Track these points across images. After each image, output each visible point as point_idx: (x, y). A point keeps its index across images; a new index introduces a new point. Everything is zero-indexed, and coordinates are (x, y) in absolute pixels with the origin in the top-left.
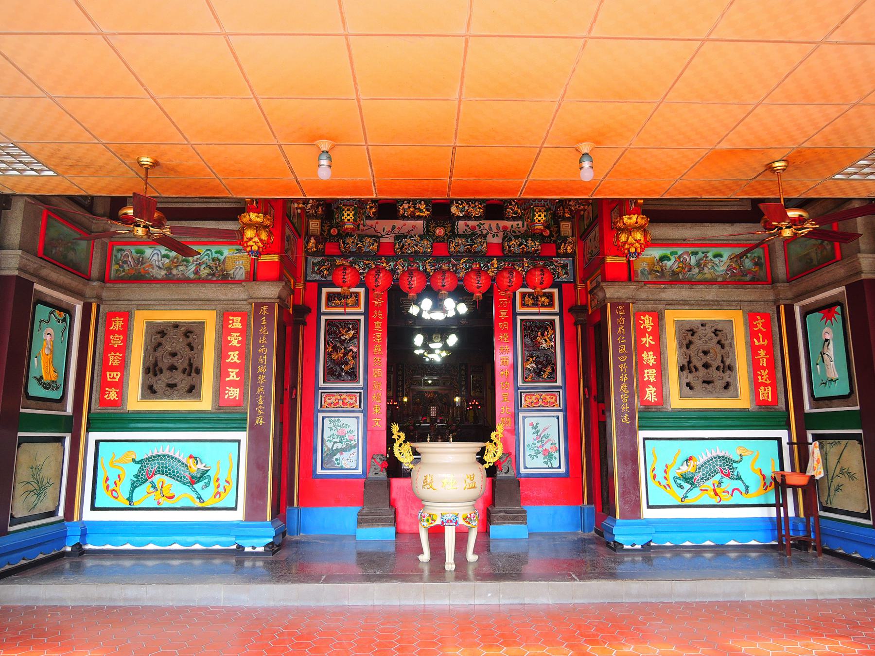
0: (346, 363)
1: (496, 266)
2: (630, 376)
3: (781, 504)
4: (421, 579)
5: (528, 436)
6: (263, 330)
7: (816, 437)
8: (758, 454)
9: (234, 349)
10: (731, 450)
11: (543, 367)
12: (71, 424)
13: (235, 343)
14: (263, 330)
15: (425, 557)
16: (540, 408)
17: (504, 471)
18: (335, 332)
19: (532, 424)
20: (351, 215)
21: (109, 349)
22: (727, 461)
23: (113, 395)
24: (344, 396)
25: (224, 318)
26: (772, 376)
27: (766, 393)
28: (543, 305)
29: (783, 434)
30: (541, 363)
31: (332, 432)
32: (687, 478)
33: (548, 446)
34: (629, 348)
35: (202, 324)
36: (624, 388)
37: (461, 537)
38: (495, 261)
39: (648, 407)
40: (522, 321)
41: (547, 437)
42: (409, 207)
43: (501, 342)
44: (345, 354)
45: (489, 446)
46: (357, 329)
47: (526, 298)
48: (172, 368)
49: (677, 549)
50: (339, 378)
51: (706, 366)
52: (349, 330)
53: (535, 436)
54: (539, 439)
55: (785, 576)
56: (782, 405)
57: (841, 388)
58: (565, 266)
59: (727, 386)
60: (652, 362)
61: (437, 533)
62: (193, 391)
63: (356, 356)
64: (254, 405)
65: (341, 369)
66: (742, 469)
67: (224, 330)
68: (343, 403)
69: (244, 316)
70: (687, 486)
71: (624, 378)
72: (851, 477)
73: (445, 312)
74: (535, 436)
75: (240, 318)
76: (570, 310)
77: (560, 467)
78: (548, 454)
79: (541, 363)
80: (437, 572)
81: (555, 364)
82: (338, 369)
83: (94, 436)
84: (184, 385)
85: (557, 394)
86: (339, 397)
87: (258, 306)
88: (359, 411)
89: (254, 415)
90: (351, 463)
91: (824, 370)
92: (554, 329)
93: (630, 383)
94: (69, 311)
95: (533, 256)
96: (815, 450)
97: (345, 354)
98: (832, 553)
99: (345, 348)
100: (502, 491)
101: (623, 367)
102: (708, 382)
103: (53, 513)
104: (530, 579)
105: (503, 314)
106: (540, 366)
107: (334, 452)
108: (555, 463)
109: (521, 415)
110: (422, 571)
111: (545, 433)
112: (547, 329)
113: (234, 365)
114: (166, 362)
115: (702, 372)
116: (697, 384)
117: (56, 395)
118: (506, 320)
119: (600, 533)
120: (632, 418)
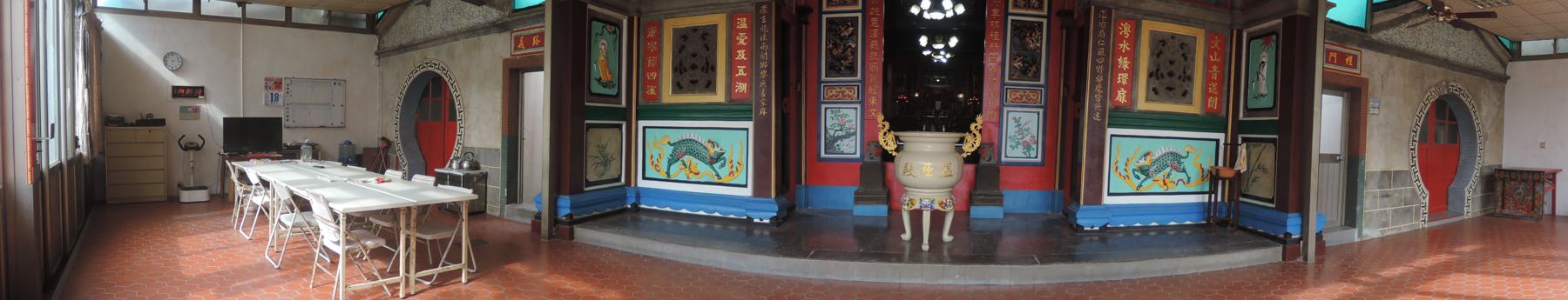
2: (1105, 78)
3: (1213, 191)
4: (900, 259)
5: (1011, 128)
6: (764, 28)
7: (1244, 140)
8: (1200, 150)
9: (741, 47)
10: (1180, 147)
11: (1027, 67)
12: (624, 114)
13: (742, 42)
14: (764, 28)
15: (907, 236)
16: (1022, 103)
21: (648, 53)
22: (1176, 157)
23: (652, 91)
26: (1220, 88)
27: (1213, 102)
29: (1221, 136)
32: (1144, 171)
33: (1027, 139)
34: (1107, 52)
35: (715, 26)
36: (1098, 88)
37: (938, 217)
39: (1117, 108)
43: (992, 40)
45: (968, 137)
46: (855, 24)
48: (694, 67)
49: (1129, 230)
50: (839, 72)
51: (1171, 74)
54: (1020, 131)
55: (1210, 252)
56: (1224, 113)
57: (1267, 102)
59: (1184, 94)
60: (1126, 67)
61: (916, 216)
62: (710, 86)
63: (854, 52)
64: (758, 97)
65: (841, 64)
66: (1187, 163)
67: (732, 32)
70: (1143, 177)
71: (1100, 79)
72: (1265, 171)
73: (944, 11)
78: (1027, 146)
80: (916, 256)
83: (642, 123)
84: (703, 82)
89: (758, 106)
90: (850, 148)
91: (1257, 87)
93: (1104, 84)
94: (618, 25)
96: (1242, 150)
98: (1244, 229)
100: (983, 174)
101: (1100, 69)
102: (1170, 89)
103: (618, 180)
104: (1009, 261)
105: (996, 12)
107: (835, 139)
108: (1033, 154)
110: (903, 249)
113: (741, 62)
114: (689, 62)
115: (1167, 79)
116: (1162, 90)
117: (613, 92)
119: (1066, 214)
120: (1103, 116)
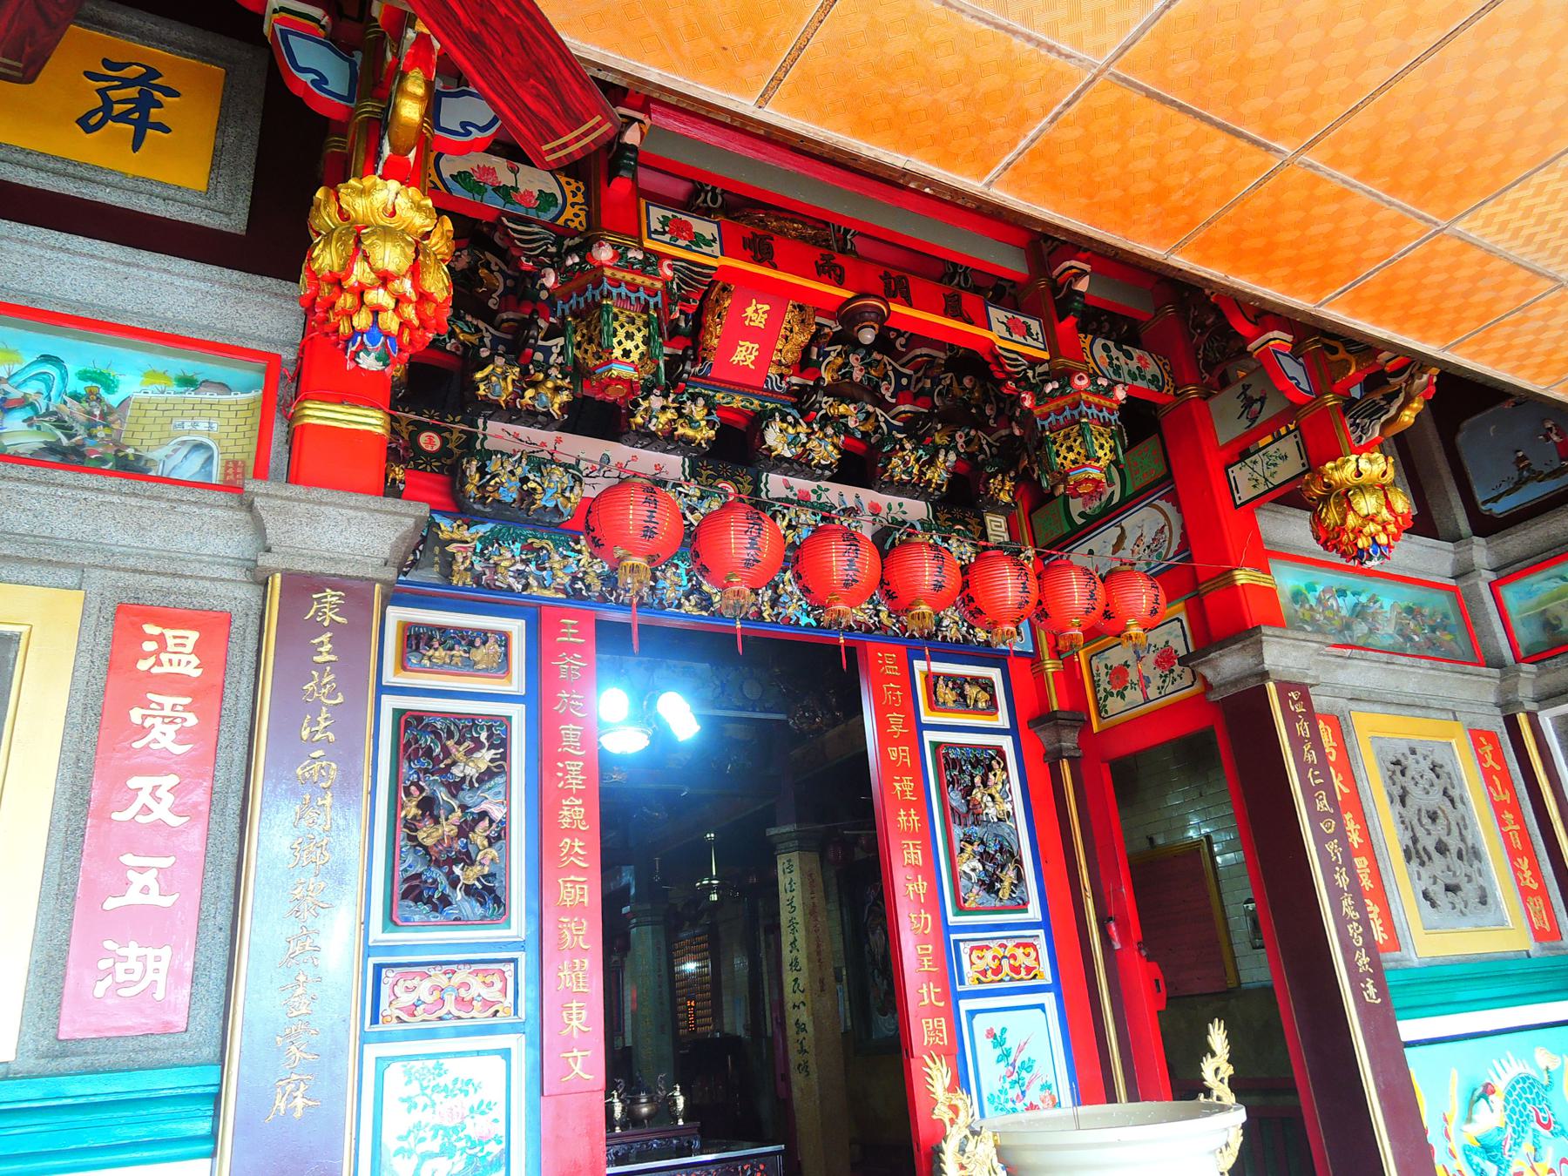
0: (467, 859)
13: (163, 738)
18: (429, 752)
19: (991, 1034)
20: (639, 337)
24: (462, 974)
25: (128, 620)
28: (977, 711)
31: (417, 1116)
42: (664, 408)
44: (464, 830)
46: (502, 744)
52: (479, 745)
53: (1002, 1069)
63: (500, 836)
68: (460, 1001)
69: (212, 627)
74: (1002, 1069)
75: (193, 636)
76: (1031, 719)
82: (442, 879)
86: (443, 981)
87: (301, 586)
88: (514, 1029)
97: (464, 830)
99: (464, 808)
111: (1023, 1057)
112: (990, 768)
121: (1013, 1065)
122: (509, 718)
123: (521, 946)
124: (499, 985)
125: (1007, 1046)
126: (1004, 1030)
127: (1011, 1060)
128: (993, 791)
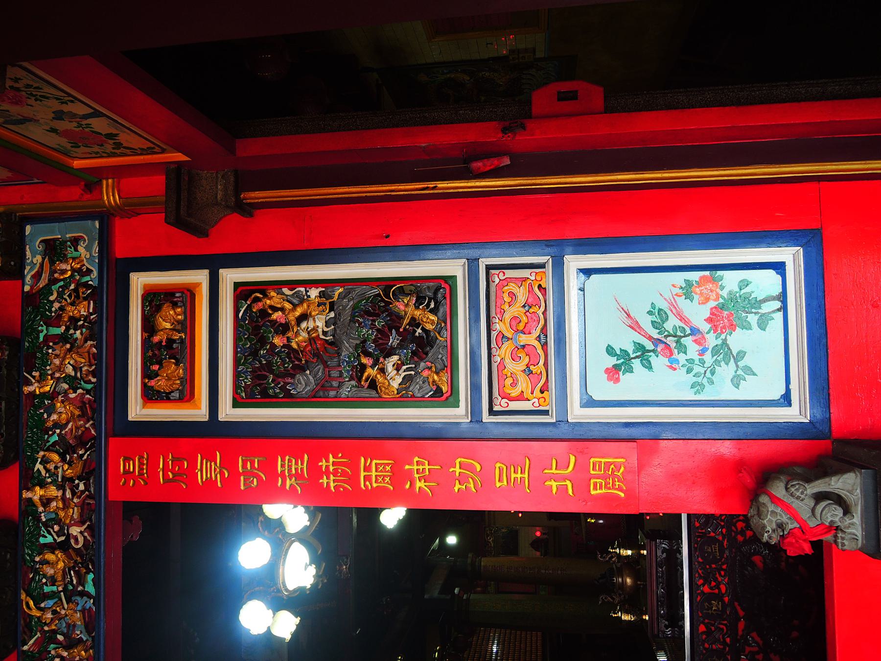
1: (53, 491)
16: (550, 341)
17: (832, 514)
19: (613, 373)
28: (188, 325)
30: (383, 334)
33: (698, 313)
38: (37, 494)
40: (237, 403)
41: (659, 316)
47: (159, 383)
53: (659, 362)
58: (54, 251)
74: (659, 362)
77: (779, 267)
79: (383, 334)
81: (386, 283)
85: (497, 277)
88: (559, 265)
92: (263, 287)
95: (70, 350)
106: (394, 340)
108: (765, 283)
109: (577, 413)
111: (646, 322)
112: (264, 314)
118: (229, 463)
121: (656, 342)
122: (237, 285)
123: (473, 264)
124: (512, 287)
125: (630, 349)
126: (610, 351)
127: (649, 346)
128: (292, 317)
